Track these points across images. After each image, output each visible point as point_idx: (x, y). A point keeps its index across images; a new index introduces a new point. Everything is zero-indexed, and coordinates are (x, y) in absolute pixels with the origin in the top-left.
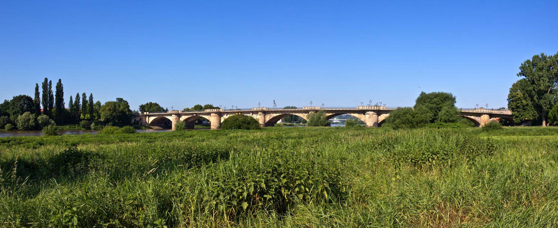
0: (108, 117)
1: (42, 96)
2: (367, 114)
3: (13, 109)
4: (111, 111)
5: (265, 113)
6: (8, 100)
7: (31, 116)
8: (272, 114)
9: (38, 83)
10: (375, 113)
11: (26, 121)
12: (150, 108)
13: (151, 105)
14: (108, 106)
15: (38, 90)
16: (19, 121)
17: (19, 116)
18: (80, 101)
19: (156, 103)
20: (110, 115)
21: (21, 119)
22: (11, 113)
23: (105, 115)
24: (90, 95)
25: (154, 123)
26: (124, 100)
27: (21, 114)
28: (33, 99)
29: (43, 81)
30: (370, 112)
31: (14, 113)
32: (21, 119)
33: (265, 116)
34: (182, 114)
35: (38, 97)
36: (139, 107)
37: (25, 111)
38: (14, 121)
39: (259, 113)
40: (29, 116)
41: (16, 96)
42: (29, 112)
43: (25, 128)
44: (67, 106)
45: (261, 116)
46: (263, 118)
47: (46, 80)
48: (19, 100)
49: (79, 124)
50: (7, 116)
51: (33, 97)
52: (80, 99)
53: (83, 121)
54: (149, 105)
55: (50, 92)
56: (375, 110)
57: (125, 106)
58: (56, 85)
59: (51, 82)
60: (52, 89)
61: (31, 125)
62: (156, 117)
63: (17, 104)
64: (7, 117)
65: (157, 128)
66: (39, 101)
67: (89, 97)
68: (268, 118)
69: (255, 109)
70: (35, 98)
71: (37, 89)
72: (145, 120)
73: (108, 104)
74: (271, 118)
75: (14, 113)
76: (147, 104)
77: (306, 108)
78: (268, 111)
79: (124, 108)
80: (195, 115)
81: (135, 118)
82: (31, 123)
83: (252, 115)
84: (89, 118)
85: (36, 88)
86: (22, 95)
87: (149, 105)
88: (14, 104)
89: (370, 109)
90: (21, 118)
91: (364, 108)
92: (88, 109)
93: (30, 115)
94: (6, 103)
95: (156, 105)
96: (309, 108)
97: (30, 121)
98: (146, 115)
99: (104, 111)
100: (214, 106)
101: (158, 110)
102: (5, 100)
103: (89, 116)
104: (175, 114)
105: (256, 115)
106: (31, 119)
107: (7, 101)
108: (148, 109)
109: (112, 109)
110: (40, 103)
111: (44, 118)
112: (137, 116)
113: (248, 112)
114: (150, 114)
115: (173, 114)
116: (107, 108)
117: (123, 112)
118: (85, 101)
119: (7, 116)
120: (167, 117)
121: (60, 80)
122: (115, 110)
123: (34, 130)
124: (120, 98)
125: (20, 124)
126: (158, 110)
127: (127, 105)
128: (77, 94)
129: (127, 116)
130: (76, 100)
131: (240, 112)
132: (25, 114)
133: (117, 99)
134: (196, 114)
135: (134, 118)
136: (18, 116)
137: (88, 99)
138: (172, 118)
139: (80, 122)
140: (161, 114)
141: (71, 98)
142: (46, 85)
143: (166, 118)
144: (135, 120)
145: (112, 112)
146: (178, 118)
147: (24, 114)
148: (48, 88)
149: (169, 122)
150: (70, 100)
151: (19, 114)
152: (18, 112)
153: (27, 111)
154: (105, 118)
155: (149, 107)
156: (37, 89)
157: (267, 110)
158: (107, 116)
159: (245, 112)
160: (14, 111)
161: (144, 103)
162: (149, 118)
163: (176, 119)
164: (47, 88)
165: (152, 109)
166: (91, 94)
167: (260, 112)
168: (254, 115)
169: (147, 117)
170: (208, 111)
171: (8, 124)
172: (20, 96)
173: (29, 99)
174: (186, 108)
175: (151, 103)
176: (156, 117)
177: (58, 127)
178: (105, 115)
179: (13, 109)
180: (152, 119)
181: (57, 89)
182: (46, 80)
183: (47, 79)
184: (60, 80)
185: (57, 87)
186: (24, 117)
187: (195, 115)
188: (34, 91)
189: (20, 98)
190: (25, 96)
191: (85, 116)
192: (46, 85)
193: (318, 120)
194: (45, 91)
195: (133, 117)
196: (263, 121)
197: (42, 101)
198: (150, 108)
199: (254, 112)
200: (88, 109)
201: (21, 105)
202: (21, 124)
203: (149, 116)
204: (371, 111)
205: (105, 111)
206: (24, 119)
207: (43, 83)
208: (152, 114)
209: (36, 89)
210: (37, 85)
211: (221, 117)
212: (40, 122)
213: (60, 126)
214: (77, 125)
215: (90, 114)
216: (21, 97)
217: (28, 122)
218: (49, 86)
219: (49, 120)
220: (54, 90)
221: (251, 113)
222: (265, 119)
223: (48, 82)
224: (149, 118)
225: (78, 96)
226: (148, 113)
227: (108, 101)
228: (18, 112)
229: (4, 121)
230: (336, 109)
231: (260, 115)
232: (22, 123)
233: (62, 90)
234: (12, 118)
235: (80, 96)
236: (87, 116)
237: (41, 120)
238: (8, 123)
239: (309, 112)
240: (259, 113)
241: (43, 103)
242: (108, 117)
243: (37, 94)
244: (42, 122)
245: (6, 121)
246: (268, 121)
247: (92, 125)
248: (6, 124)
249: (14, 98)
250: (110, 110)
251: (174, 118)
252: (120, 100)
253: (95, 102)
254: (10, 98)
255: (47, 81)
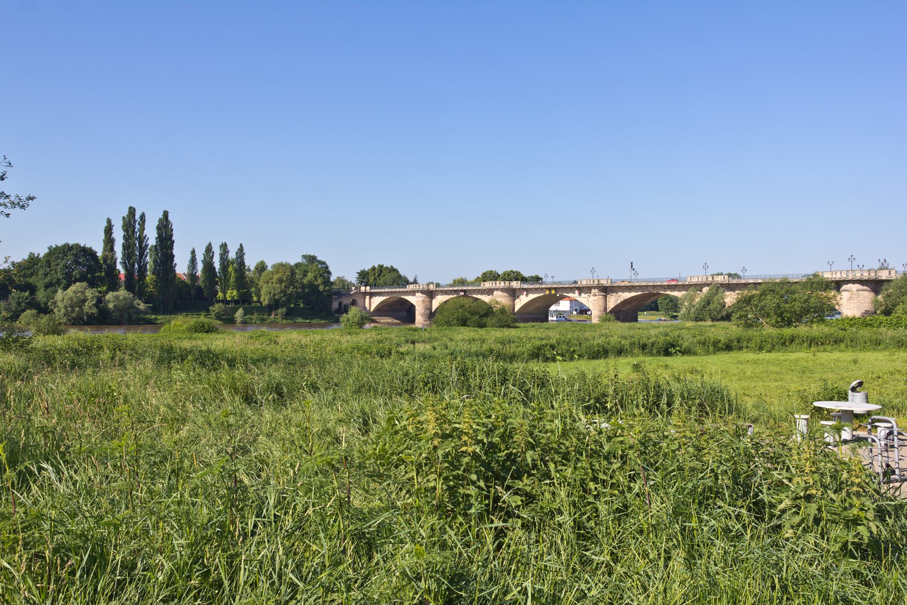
0: (276, 297)
1: (121, 248)
2: (845, 291)
3: (46, 275)
4: (283, 285)
5: (606, 290)
6: (39, 254)
7: (89, 293)
8: (620, 293)
9: (110, 218)
10: (865, 288)
11: (76, 303)
12: (379, 276)
13: (381, 272)
14: (277, 272)
15: (111, 233)
16: (59, 304)
17: (60, 291)
18: (214, 260)
19: (392, 267)
20: (280, 293)
21: (63, 299)
22: (40, 284)
23: (270, 293)
24: (239, 247)
25: (382, 310)
26: (318, 258)
27: (65, 288)
28: (100, 254)
29: (125, 213)
30: (850, 286)
31: (47, 287)
32: (63, 299)
33: (606, 297)
34: (436, 291)
35: (112, 249)
36: (357, 276)
37: (76, 281)
38: (46, 304)
39: (593, 291)
40: (83, 292)
41: (57, 246)
42: (84, 284)
43: (74, 319)
44: (181, 268)
45: (596, 298)
46: (601, 302)
47: (132, 211)
48: (61, 255)
49: (208, 311)
50: (28, 292)
51: (99, 249)
52: (213, 256)
53: (217, 306)
54: (376, 271)
55: (142, 239)
56: (866, 281)
57: (317, 272)
58: (157, 223)
59: (143, 217)
60: (145, 232)
61: (88, 313)
62: (385, 298)
63: (58, 265)
64: (27, 294)
65: (389, 321)
66: (112, 257)
67: (237, 253)
68: (613, 301)
69: (584, 283)
70: (104, 250)
71: (109, 230)
72: (363, 304)
73: (280, 267)
74: (619, 302)
75: (47, 287)
76: (374, 269)
77: (695, 280)
78: (613, 287)
79: (316, 278)
80: (462, 293)
81: (340, 300)
82: (89, 307)
83: (580, 294)
84: (235, 298)
85: (106, 228)
86: (71, 242)
87: (376, 271)
88: (48, 263)
89: (850, 278)
90: (63, 297)
91: (834, 276)
92: (232, 280)
93: (87, 291)
94: (33, 260)
95: (393, 270)
96: (700, 280)
97: (86, 304)
98: (365, 294)
99: (268, 283)
100: (526, 274)
101: (394, 282)
102: (31, 253)
103: (235, 293)
104: (423, 292)
105: (586, 295)
106: (87, 300)
107: (36, 255)
108: (375, 279)
109: (285, 279)
110: (115, 263)
111: (121, 298)
112: (345, 295)
113: (571, 288)
114: (372, 291)
115: (418, 291)
116: (276, 277)
117: (312, 287)
118: (208, 266)
119: (28, 292)
120: (406, 297)
121: (166, 214)
122: (291, 280)
123: (96, 324)
124: (310, 256)
125: (59, 311)
126: (394, 282)
127: (325, 271)
128: (207, 244)
129: (320, 293)
130: (205, 258)
131: (555, 289)
132: (73, 288)
133: (304, 257)
134: (465, 291)
135: (337, 299)
136: (56, 291)
137: (232, 255)
138: (417, 300)
139: (210, 308)
140: (395, 292)
141: (193, 252)
142: (132, 222)
143: (407, 301)
144: (340, 304)
145: (285, 287)
146: (427, 299)
147: (71, 288)
148: (136, 230)
149: (411, 308)
150: (189, 259)
151: (61, 286)
152: (58, 282)
153: (80, 280)
154: (270, 299)
155: (377, 275)
156: (109, 230)
157: (609, 284)
158: (274, 295)
159: (565, 288)
160: (47, 280)
161: (367, 267)
162: (370, 298)
163: (424, 301)
164: (135, 228)
165: (382, 279)
166: (241, 245)
167: (595, 288)
168: (583, 295)
169: (368, 297)
170: (488, 285)
171: (28, 311)
172: (67, 245)
173: (88, 253)
174: (457, 277)
175: (381, 267)
176: (385, 298)
177: (159, 317)
178: (270, 293)
179: (46, 275)
180: (377, 301)
181: (158, 233)
182: (132, 211)
183: (134, 209)
184: (166, 214)
185: (159, 228)
186: (72, 294)
187: (462, 293)
188: (102, 236)
189: (66, 250)
190: (77, 245)
191: (225, 293)
192: (132, 222)
193: (704, 307)
194: (130, 237)
195: (334, 297)
196: (602, 308)
197: (122, 259)
198: (379, 276)
199: (583, 287)
200: (232, 280)
201: (66, 267)
202: (63, 311)
203: (372, 295)
204: (854, 282)
205: (270, 283)
206: (71, 299)
207: (124, 218)
208: (376, 291)
209: (105, 230)
210: (109, 221)
211: (515, 300)
212: (111, 306)
213: (164, 314)
214: (203, 314)
215: (238, 290)
216: (66, 248)
217: (80, 307)
218: (139, 224)
219: (132, 303)
220: (151, 236)
221: (576, 292)
222: (606, 304)
223: (137, 217)
224: (370, 298)
225: (209, 249)
226: (368, 288)
227: (279, 261)
228: (58, 282)
229: (19, 304)
230: (757, 279)
231: (595, 295)
232: (66, 307)
233: (171, 236)
234: (41, 295)
235: (214, 249)
236: (232, 293)
237: (113, 302)
238: (28, 308)
239: (702, 288)
240: (593, 291)
241: (125, 263)
242: (276, 297)
243: (109, 242)
244: (115, 306)
245: (23, 304)
246: (613, 309)
247: (239, 313)
248: (24, 311)
249: (50, 249)
250: (280, 281)
251: (420, 299)
252: (312, 259)
253: (251, 262)
254: (42, 251)
255: (134, 215)
